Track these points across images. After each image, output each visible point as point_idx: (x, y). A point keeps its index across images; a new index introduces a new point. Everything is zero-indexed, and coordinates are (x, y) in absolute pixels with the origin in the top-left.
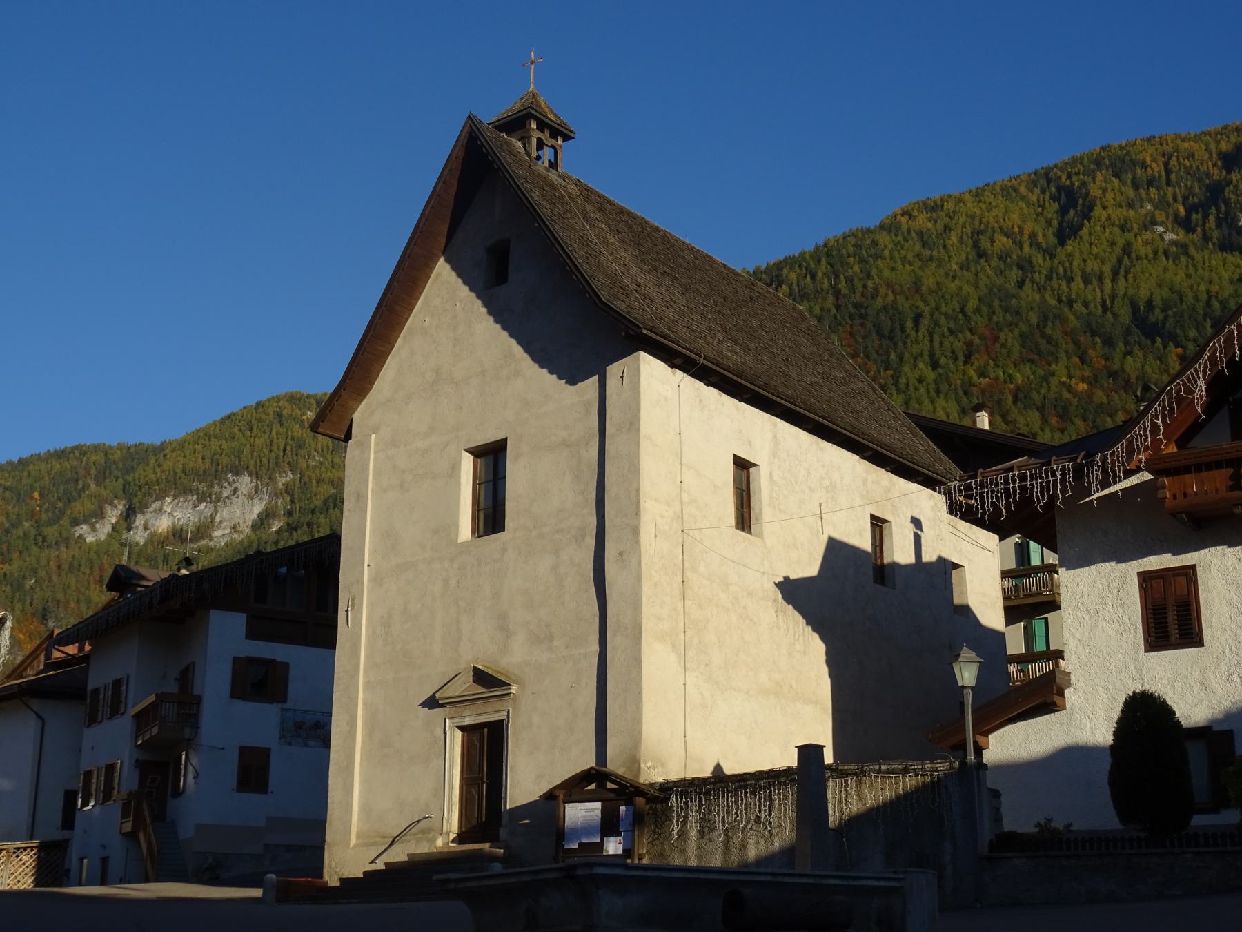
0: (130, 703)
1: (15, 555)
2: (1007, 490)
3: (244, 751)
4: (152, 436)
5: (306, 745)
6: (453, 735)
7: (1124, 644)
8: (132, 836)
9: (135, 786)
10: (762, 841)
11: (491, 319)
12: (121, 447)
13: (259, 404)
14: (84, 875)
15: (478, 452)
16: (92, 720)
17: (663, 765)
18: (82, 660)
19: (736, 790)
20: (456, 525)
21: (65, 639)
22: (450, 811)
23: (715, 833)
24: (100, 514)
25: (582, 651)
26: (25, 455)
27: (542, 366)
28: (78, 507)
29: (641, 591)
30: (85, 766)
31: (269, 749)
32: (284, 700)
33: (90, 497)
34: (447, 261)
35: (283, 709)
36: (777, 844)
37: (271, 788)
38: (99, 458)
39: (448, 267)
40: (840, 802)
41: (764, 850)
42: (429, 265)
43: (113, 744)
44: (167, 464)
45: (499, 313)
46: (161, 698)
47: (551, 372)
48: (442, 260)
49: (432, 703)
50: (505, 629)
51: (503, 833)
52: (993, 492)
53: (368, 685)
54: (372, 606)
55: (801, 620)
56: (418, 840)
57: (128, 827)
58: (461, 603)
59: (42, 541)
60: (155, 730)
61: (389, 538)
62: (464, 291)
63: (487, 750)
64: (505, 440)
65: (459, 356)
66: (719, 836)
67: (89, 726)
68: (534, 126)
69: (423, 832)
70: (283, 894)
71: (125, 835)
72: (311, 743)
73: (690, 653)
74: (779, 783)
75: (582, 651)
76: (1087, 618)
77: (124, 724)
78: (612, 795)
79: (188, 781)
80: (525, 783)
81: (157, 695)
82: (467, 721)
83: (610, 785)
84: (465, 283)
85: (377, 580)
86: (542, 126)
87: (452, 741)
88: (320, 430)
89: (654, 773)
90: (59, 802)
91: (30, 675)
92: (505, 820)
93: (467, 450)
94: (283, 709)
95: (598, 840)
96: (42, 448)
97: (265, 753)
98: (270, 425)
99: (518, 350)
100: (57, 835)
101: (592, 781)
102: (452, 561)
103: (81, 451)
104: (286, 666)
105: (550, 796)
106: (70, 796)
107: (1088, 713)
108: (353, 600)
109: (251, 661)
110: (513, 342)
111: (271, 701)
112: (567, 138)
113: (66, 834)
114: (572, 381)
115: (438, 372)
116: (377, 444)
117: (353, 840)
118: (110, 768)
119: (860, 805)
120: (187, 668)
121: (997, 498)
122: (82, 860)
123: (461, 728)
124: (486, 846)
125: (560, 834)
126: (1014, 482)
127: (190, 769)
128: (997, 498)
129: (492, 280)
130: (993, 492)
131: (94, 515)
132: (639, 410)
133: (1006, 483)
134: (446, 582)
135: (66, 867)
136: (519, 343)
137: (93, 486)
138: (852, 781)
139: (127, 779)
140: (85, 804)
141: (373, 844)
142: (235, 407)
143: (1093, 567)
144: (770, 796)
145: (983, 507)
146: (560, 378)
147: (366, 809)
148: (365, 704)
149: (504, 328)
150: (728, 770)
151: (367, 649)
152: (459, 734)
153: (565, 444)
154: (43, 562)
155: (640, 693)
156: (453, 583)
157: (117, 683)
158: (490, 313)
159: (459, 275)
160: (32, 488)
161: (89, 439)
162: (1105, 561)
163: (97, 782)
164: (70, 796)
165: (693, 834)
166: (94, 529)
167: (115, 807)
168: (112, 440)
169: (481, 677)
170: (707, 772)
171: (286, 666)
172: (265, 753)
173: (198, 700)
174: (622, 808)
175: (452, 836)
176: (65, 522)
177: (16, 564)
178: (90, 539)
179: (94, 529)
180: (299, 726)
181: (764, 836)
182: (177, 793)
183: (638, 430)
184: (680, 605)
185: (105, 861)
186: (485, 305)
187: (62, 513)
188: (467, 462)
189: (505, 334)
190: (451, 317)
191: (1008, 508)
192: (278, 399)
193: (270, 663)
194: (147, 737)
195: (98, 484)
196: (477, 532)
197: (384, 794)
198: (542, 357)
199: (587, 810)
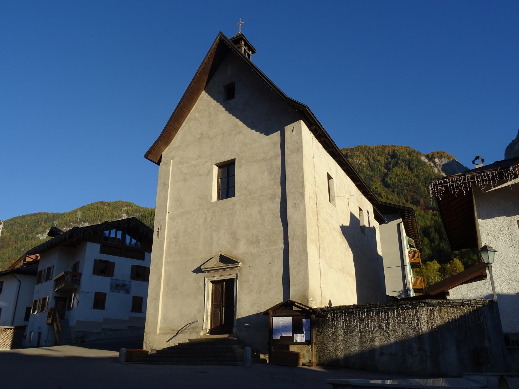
0: (54, 275)
1: (19, 242)
2: (465, 183)
3: (97, 294)
4: (62, 212)
5: (119, 292)
6: (208, 285)
7: (513, 251)
8: (51, 325)
9: (53, 306)
10: (384, 338)
11: (227, 112)
12: (52, 213)
13: (92, 204)
14: (32, 337)
15: (220, 166)
16: (39, 282)
17: (315, 300)
18: (36, 262)
19: (367, 311)
20: (211, 195)
21: (30, 253)
22: (207, 319)
23: (354, 333)
24: (44, 231)
25: (275, 247)
26: (24, 214)
27: (252, 129)
28: (38, 229)
29: (305, 220)
30: (35, 298)
31: (106, 294)
32: (112, 276)
33: (42, 227)
34: (206, 92)
35: (112, 279)
36: (393, 339)
37: (106, 307)
38: (45, 216)
39: (207, 94)
40: (431, 319)
41: (384, 341)
42: (198, 93)
43: (47, 291)
44: (65, 219)
45: (230, 110)
46: (66, 273)
47: (257, 131)
48: (204, 92)
49: (199, 270)
50: (234, 238)
51: (234, 330)
52: (458, 184)
53: (167, 263)
54: (169, 229)
55: (347, 243)
56: (191, 332)
57: (50, 321)
58: (213, 228)
59: (27, 238)
60: (63, 285)
61: (178, 201)
62: (214, 103)
63: (225, 293)
64: (235, 159)
65: (212, 128)
66: (356, 335)
67: (37, 284)
68: (243, 43)
69: (193, 328)
70: (129, 359)
71: (49, 324)
72: (121, 292)
73: (321, 251)
74: (394, 309)
75: (275, 247)
76: (494, 240)
77: (51, 283)
78: (299, 314)
79: (74, 303)
80: (246, 306)
81: (65, 272)
82: (216, 279)
83: (295, 308)
84: (214, 99)
85: (172, 218)
86: (246, 44)
87: (208, 288)
88: (149, 157)
89: (317, 302)
90: (24, 312)
91: (17, 267)
92: (235, 324)
93: (215, 165)
94: (112, 279)
95: (291, 335)
96: (29, 213)
97: (104, 295)
98: (95, 210)
99: (240, 123)
100: (22, 323)
101: (286, 307)
102: (208, 210)
103: (40, 214)
104: (114, 263)
105: (266, 313)
106: (28, 309)
107: (498, 281)
108: (161, 227)
109: (101, 261)
110: (238, 120)
111: (108, 276)
112: (253, 52)
113: (25, 323)
114: (267, 133)
115: (202, 134)
116: (173, 164)
117: (158, 331)
118: (45, 299)
119: (441, 321)
120: (76, 264)
121: (461, 186)
122: (31, 332)
123: (212, 282)
124: (226, 336)
125: (270, 330)
126: (468, 179)
127: (76, 299)
128: (461, 186)
129: (227, 97)
130: (458, 184)
131: (43, 232)
132: (302, 143)
133: (464, 180)
134: (206, 219)
135: (25, 335)
136: (241, 120)
137: (43, 224)
138: (436, 309)
139: (51, 303)
140: (34, 312)
141: (168, 333)
142: (85, 204)
143: (494, 219)
144: (388, 315)
145: (454, 189)
146: (261, 133)
147: (164, 318)
148: (165, 271)
149: (233, 115)
150: (334, 304)
151: (167, 247)
152: (211, 284)
153: (264, 159)
154: (27, 244)
155: (307, 267)
156: (209, 219)
157: (49, 269)
158: (226, 110)
159: (212, 97)
160: (26, 224)
161: (43, 211)
162: (500, 216)
163: (39, 304)
164: (28, 309)
165: (341, 333)
166: (42, 236)
167: (45, 314)
168: (50, 212)
169: (223, 259)
170: (325, 305)
171: (114, 263)
172: (104, 295)
173: (80, 275)
174: (304, 320)
175: (208, 331)
176: (34, 233)
177: (19, 244)
178: (41, 238)
179: (42, 236)
180: (117, 285)
181: (384, 335)
182: (70, 309)
183: (302, 152)
184: (317, 229)
185: (40, 333)
186: (224, 107)
187: (34, 231)
188: (215, 169)
189: (234, 117)
190: (208, 113)
191: (466, 191)
192: (97, 203)
193: (108, 262)
194: (60, 288)
195: (45, 223)
196: (218, 198)
197: (174, 311)
198: (252, 124)
199: (284, 321)
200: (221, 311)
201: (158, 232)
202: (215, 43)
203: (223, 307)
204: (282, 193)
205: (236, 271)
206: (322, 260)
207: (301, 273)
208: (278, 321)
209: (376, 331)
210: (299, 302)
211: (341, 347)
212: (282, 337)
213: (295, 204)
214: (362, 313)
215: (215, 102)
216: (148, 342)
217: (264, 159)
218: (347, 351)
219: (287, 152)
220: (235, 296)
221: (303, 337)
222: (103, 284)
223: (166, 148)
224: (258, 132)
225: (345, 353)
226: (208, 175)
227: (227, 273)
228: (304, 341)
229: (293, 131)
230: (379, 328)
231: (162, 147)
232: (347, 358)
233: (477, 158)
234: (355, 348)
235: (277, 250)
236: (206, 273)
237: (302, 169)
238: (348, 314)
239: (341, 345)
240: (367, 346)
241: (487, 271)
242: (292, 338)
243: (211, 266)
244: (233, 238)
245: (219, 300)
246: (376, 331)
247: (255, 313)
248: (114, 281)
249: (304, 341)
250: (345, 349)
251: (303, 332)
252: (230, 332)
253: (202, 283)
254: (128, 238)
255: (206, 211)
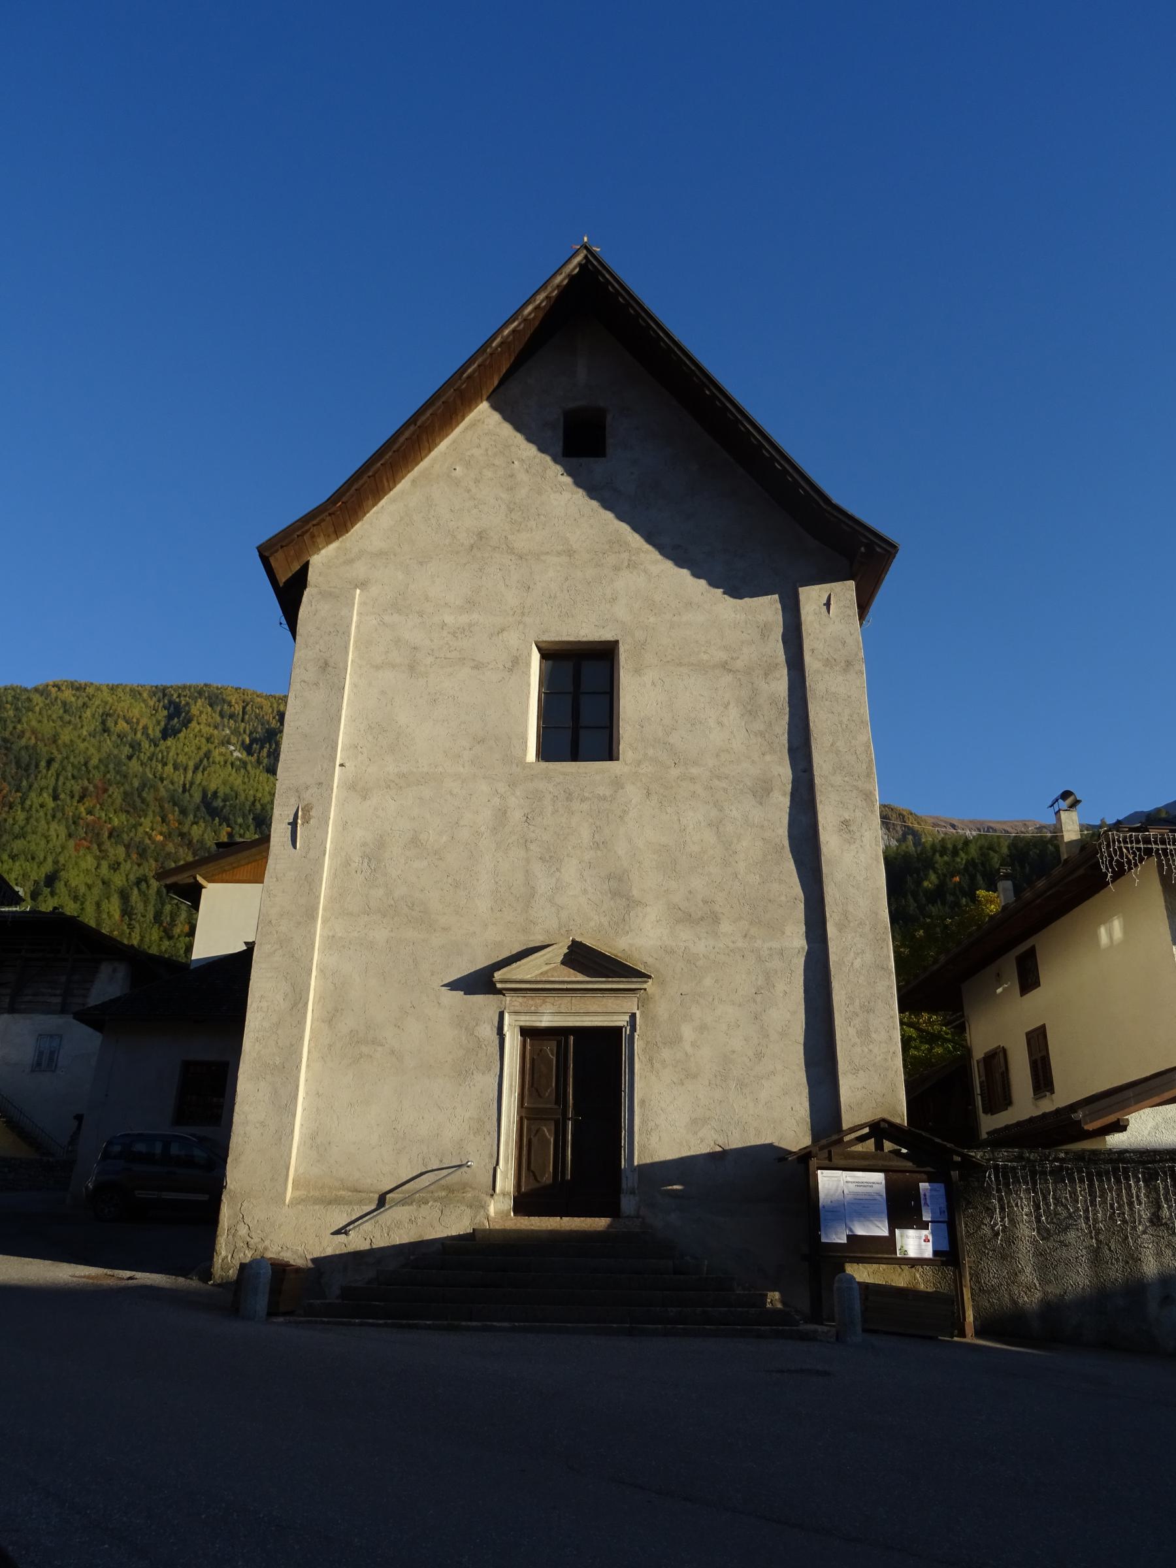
15: (553, 654)
23: (1071, 1236)
25: (775, 945)
47: (696, 575)
50: (619, 890)
51: (628, 1204)
54: (344, 826)
78: (909, 1165)
95: (884, 1232)
102: (512, 785)
108: (307, 809)
114: (736, 591)
116: (363, 604)
129: (577, 443)
146: (713, 584)
147: (317, 1143)
148: (321, 971)
151: (331, 887)
153: (725, 666)
156: (517, 816)
169: (582, 957)
174: (924, 1186)
186: (570, 472)
188: (536, 656)
189: (609, 515)
199: (859, 1184)
200: (560, 1134)
201: (294, 825)
203: (565, 1119)
204: (795, 782)
205: (630, 1004)
207: (874, 1036)
208: (832, 1183)
209: (1144, 1232)
211: (1029, 1275)
212: (852, 1238)
213: (846, 823)
214: (1099, 1175)
215: (530, 450)
216: (243, 1231)
217: (725, 666)
218: (1053, 1290)
219: (811, 662)
220: (625, 1086)
221: (927, 1240)
223: (329, 543)
224: (703, 582)
225: (1045, 1293)
226: (510, 670)
227: (594, 1008)
228: (928, 1253)
229: (828, 604)
230: (1151, 1221)
231: (320, 540)
232: (1052, 1309)
233: (1066, 795)
234: (1078, 1278)
235: (781, 953)
236: (508, 999)
238: (1052, 1173)
239: (1028, 1270)
240: (1115, 1273)
242: (889, 1243)
243: (528, 977)
244: (615, 894)
245: (550, 1092)
246: (1144, 1232)
247: (704, 1149)
249: (928, 1253)
250: (1044, 1281)
251: (923, 1226)
252: (610, 1208)
253: (488, 1032)
255: (502, 787)
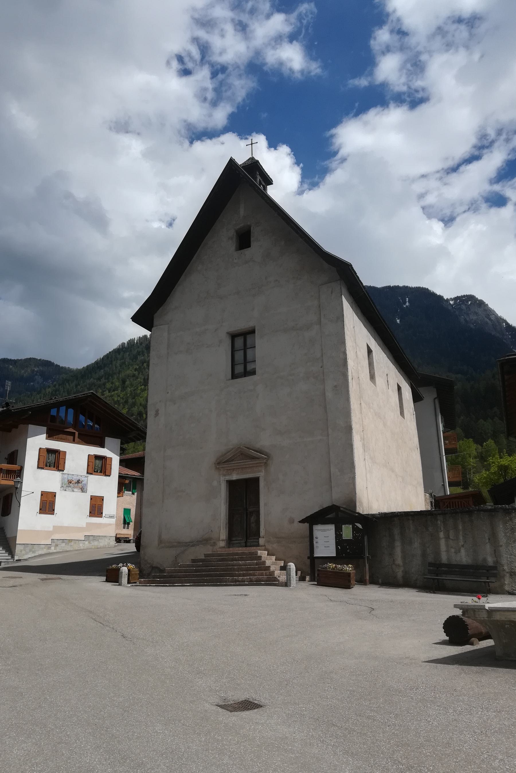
3: (43, 494)
5: (73, 491)
72: (75, 490)
82: (235, 477)
97: (54, 495)
104: (65, 453)
172: (54, 495)
202: (501, 599)
206: (366, 454)
210: (344, 506)
213: (336, 386)
222: (50, 480)
237: (343, 342)
241: (316, 583)
248: (66, 476)
254: (82, 418)
